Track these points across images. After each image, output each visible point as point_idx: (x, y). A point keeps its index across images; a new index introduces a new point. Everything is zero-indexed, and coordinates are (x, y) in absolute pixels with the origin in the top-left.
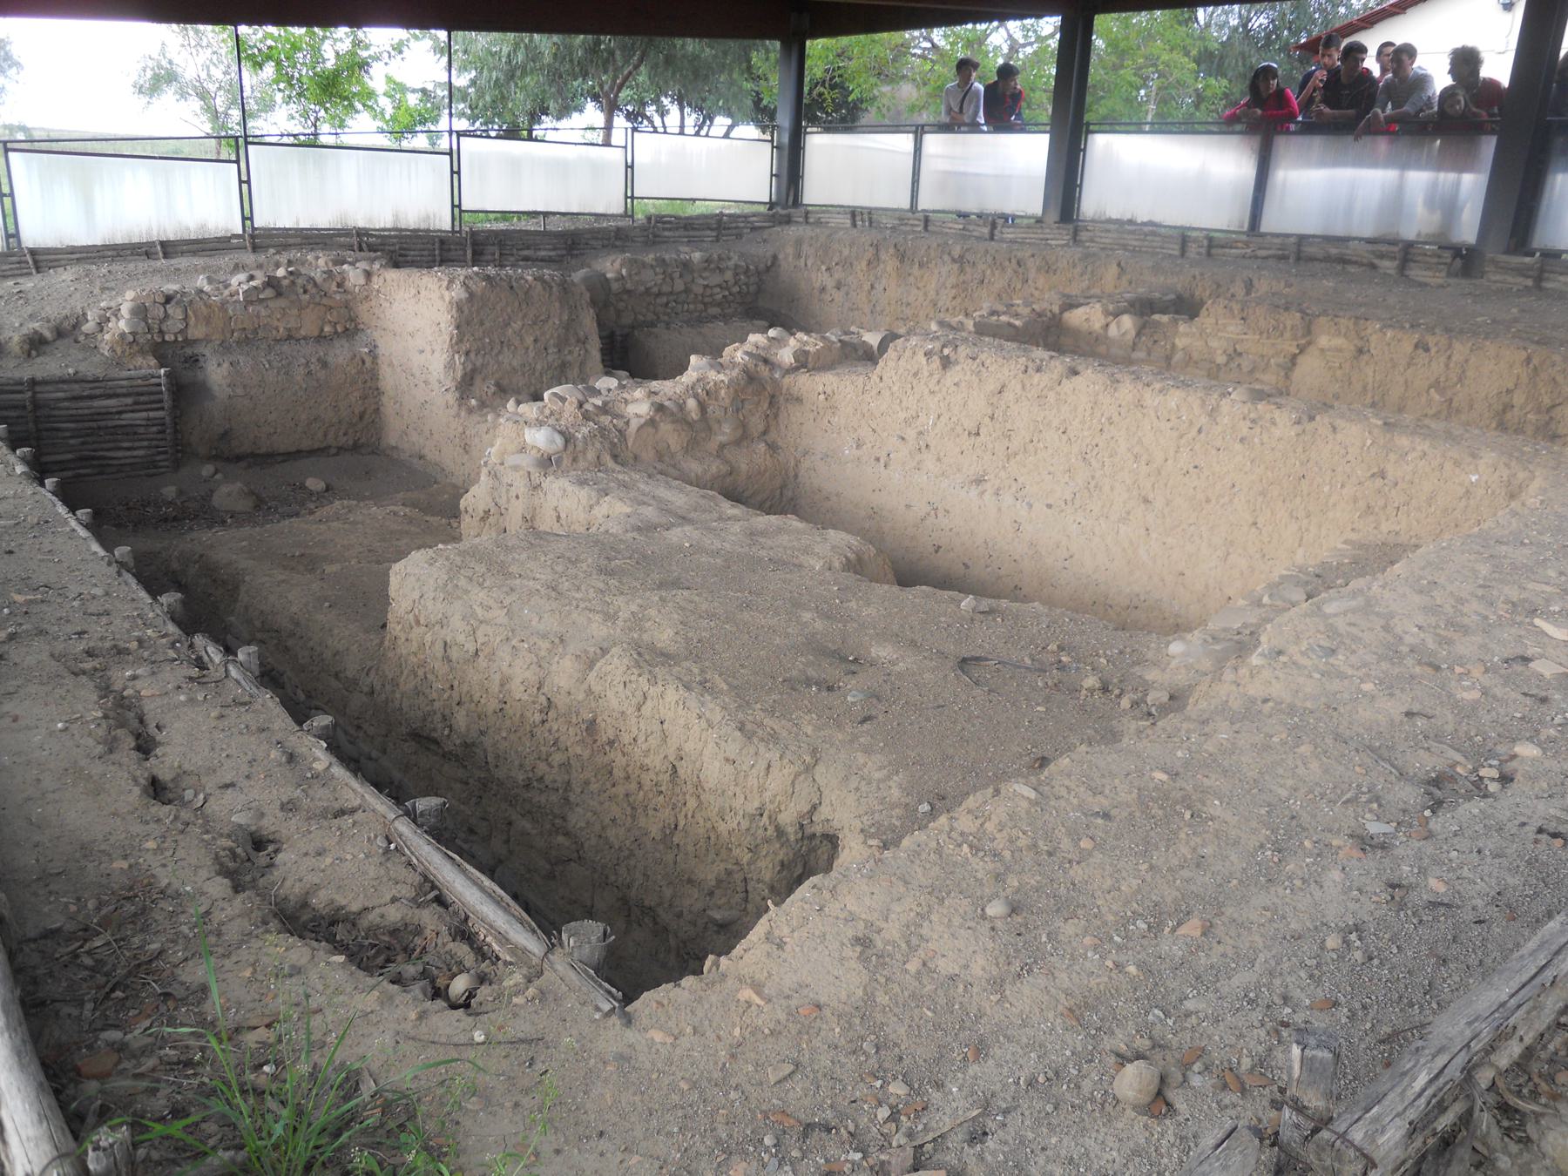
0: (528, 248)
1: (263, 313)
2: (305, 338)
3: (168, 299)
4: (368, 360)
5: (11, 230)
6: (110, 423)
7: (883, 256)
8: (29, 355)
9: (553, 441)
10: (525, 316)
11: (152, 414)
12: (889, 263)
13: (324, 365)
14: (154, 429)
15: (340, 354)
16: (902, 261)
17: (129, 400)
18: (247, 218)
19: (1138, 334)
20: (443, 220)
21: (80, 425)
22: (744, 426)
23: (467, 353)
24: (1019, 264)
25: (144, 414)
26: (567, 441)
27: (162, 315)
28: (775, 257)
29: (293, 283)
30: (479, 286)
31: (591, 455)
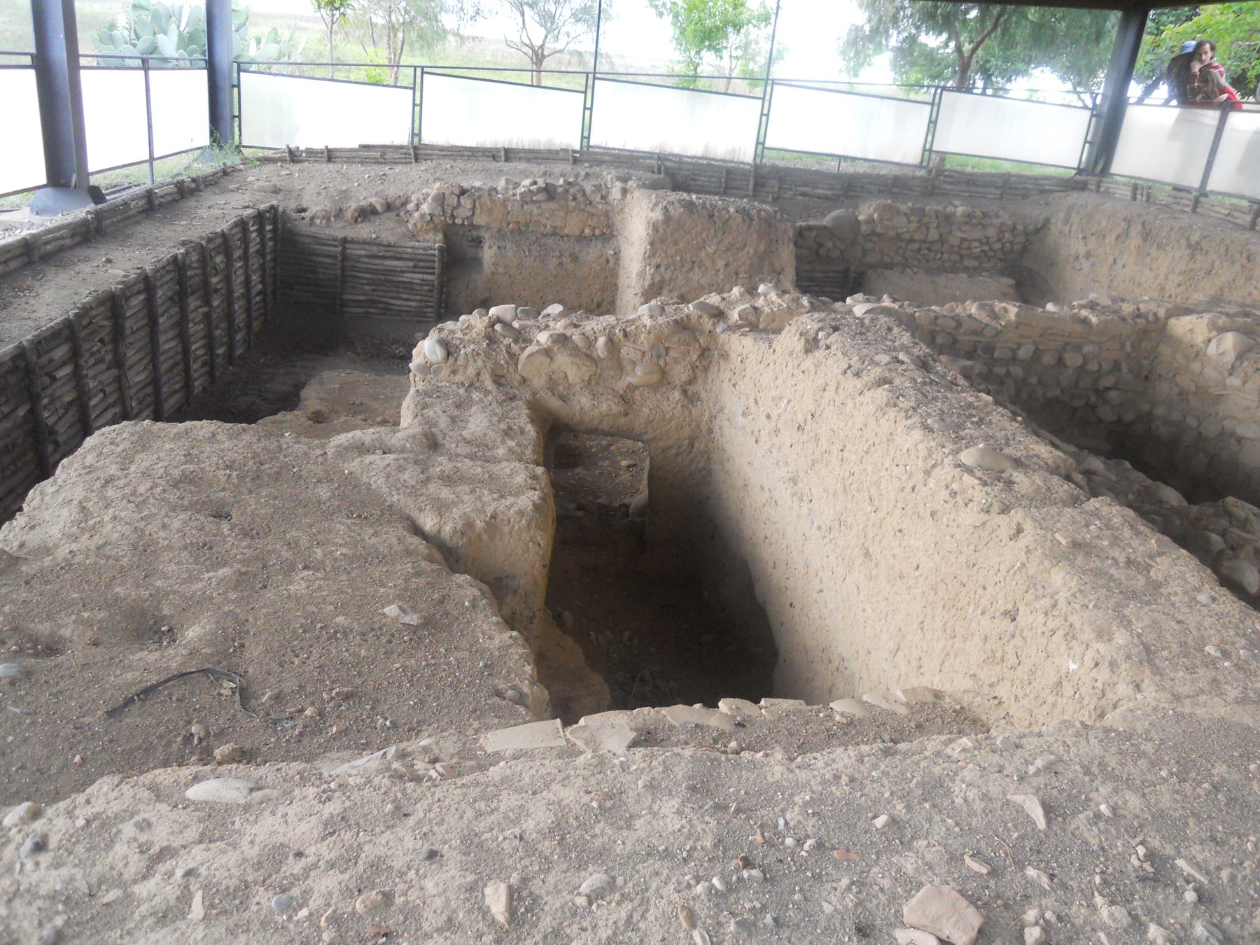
0: (807, 185)
1: (536, 211)
2: (568, 236)
3: (463, 192)
4: (612, 261)
5: (416, 131)
6: (395, 279)
7: (1133, 233)
8: (356, 221)
9: (434, 352)
10: (720, 242)
11: (426, 277)
12: (1135, 240)
13: (575, 258)
14: (426, 288)
15: (591, 253)
16: (1145, 240)
17: (411, 264)
18: (585, 138)
19: (1241, 356)
20: (745, 152)
21: (374, 277)
22: (664, 373)
23: (658, 267)
24: (1249, 259)
25: (421, 276)
26: (449, 354)
27: (455, 204)
28: (1047, 221)
29: (567, 191)
30: (677, 211)
31: (471, 371)
